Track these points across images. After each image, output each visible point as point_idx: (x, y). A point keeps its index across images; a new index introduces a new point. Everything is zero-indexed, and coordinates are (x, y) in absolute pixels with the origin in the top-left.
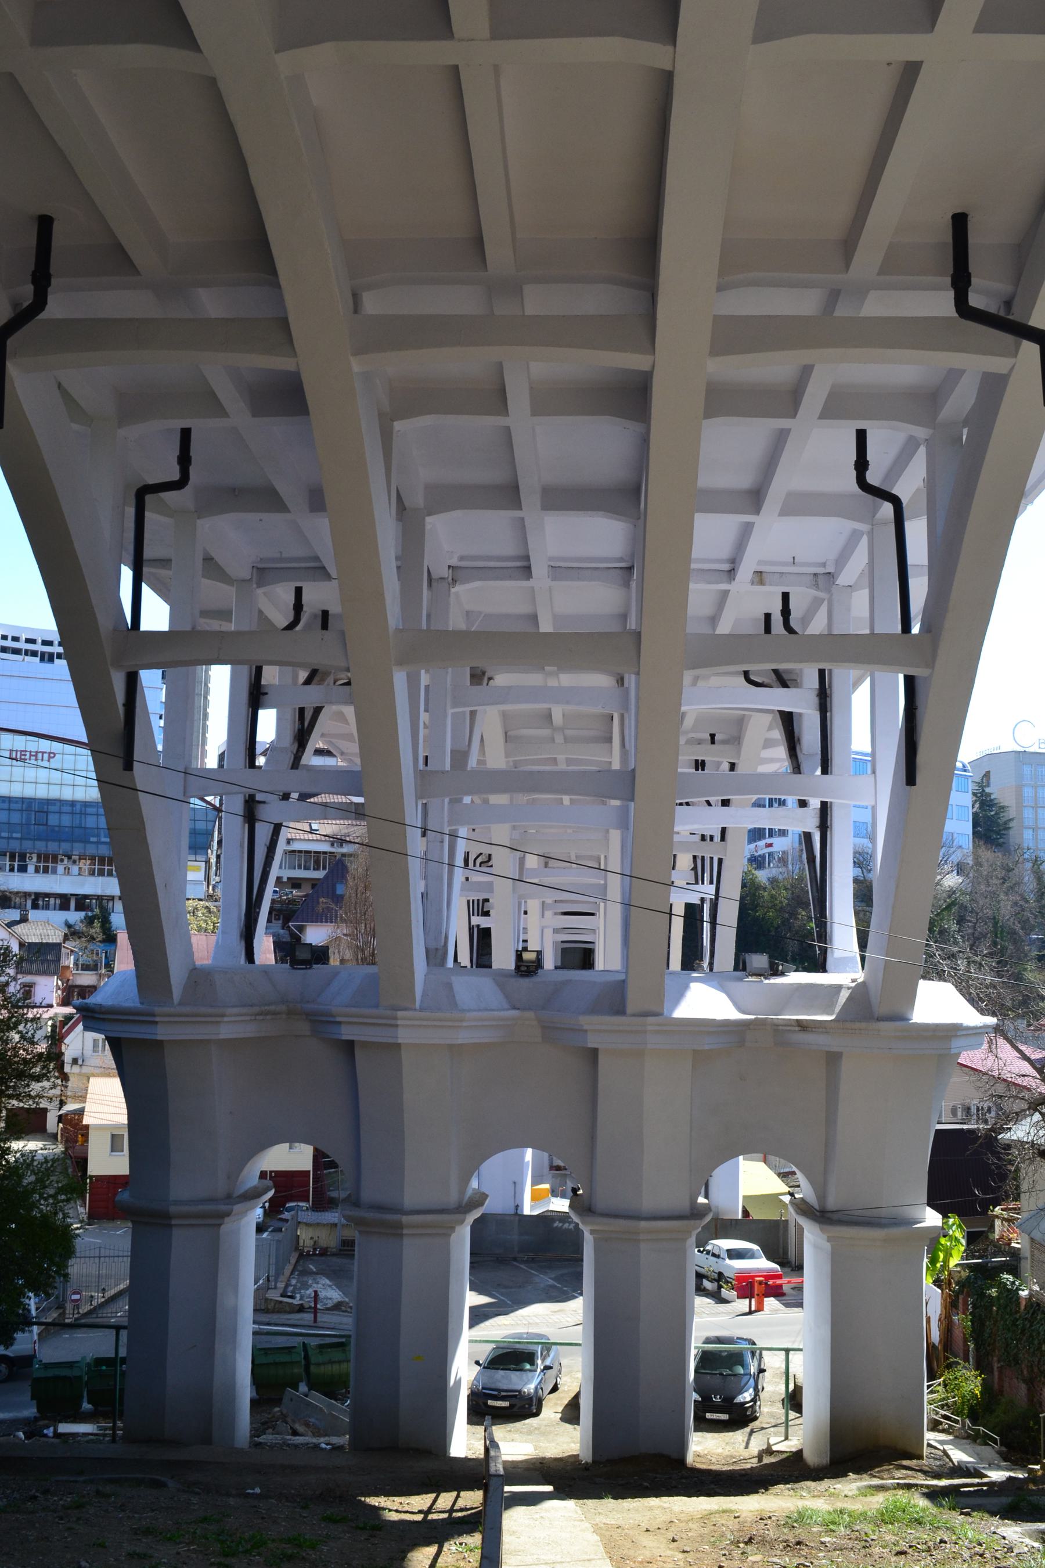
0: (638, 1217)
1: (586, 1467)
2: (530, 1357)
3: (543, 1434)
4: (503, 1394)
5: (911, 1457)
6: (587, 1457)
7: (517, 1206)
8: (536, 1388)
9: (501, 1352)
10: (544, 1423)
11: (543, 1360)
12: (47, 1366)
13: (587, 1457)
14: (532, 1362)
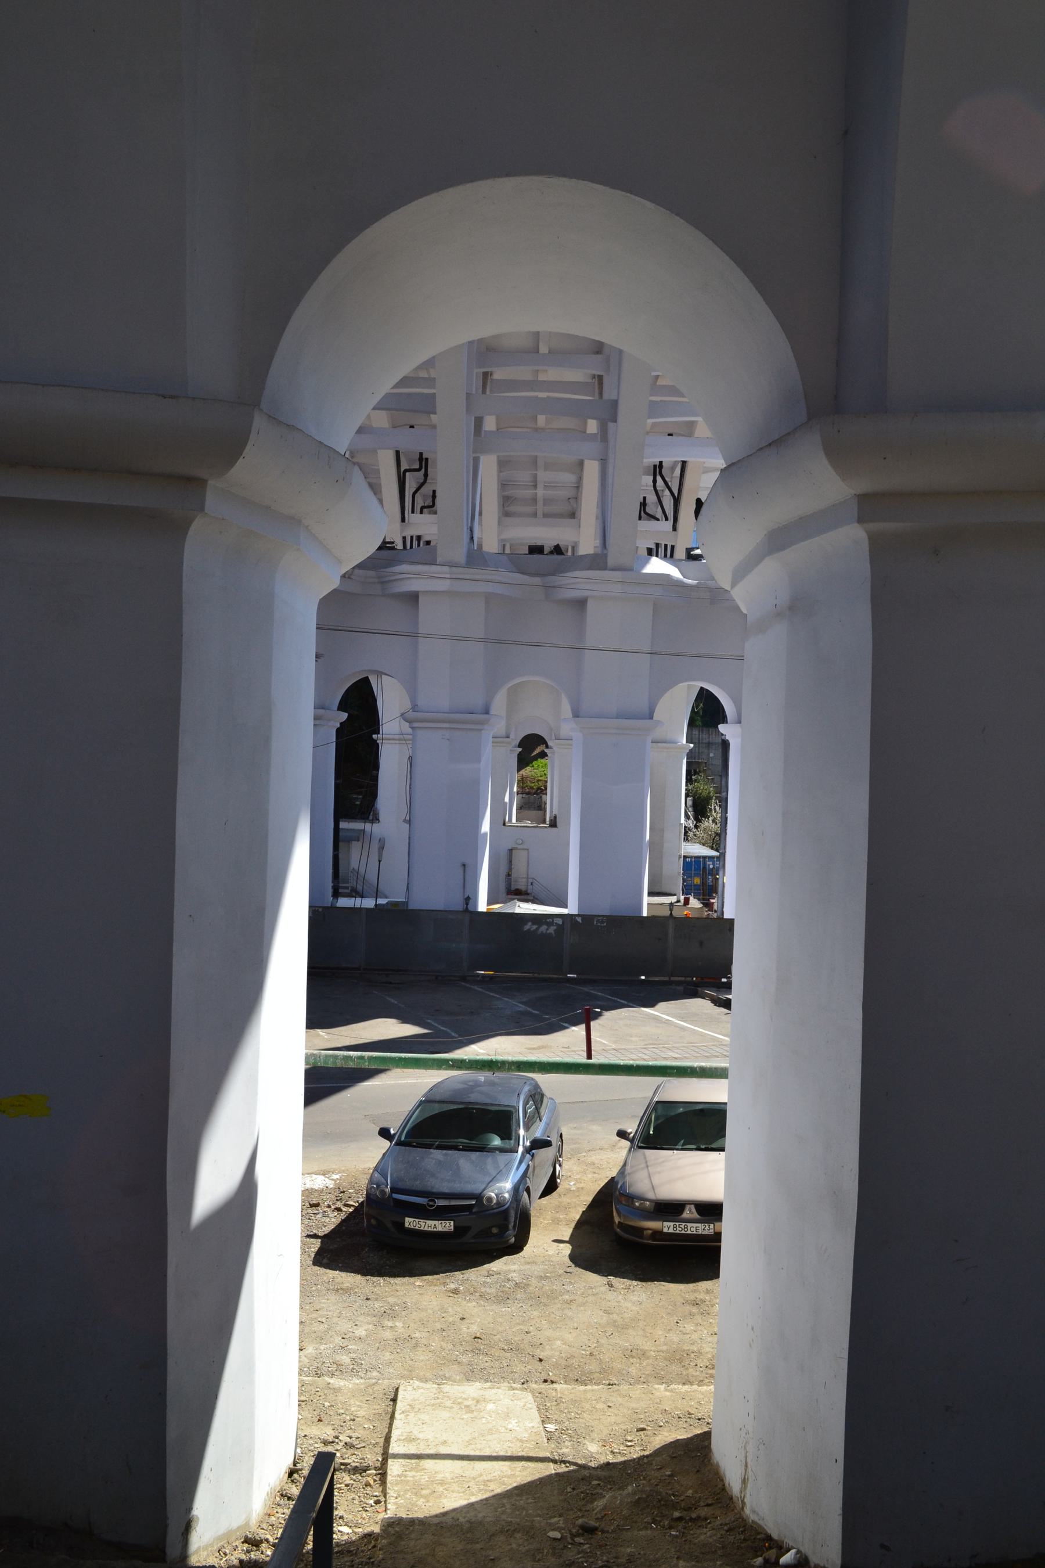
2: (501, 1122)
3: (537, 1300)
4: (441, 1203)
7: (467, 900)
8: (516, 1189)
9: (436, 1109)
10: (537, 1269)
11: (527, 1128)
14: (506, 1130)
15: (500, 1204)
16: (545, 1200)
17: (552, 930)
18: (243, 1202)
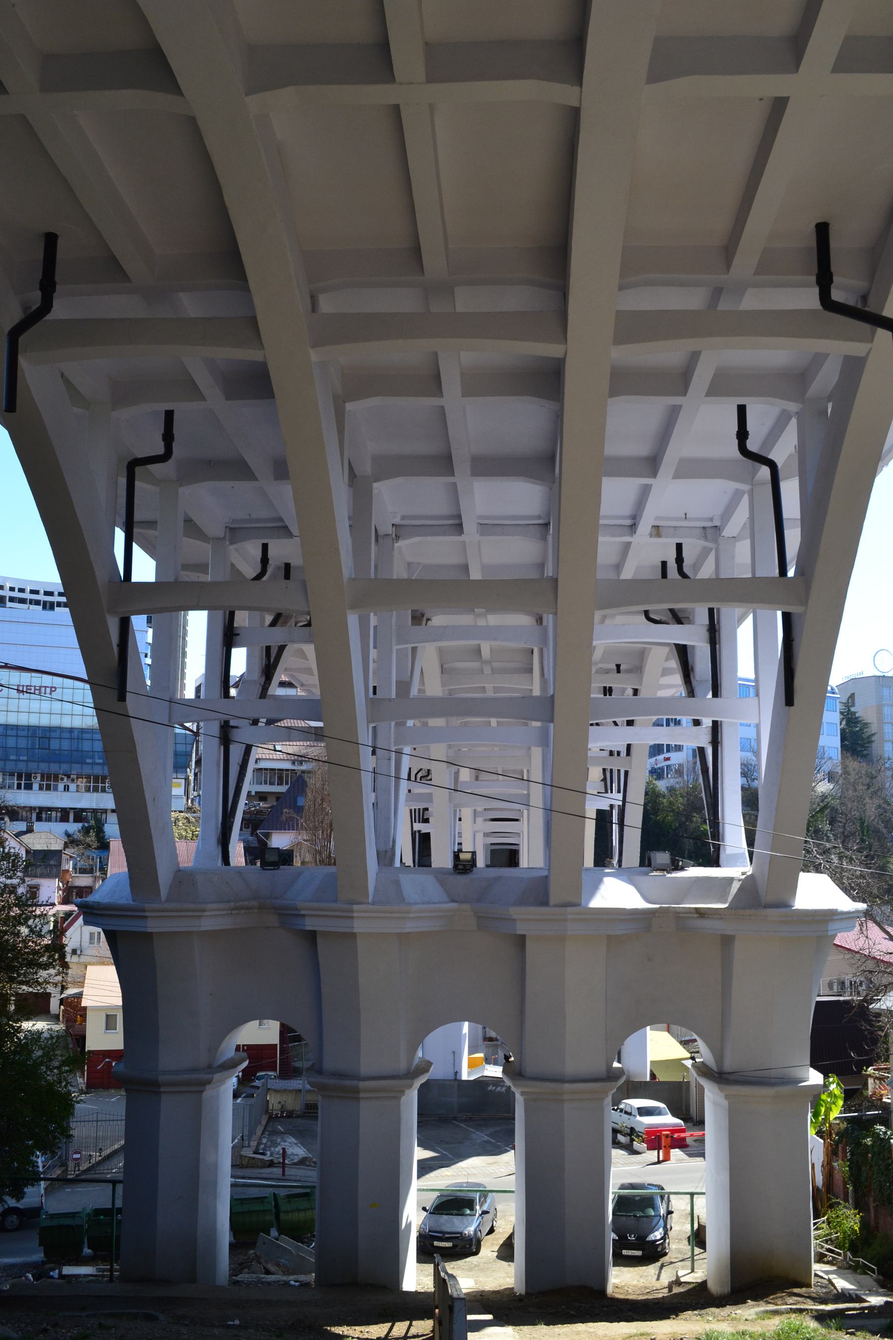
0: (561, 1080)
1: (520, 1298)
2: (469, 1204)
4: (447, 1236)
5: (801, 1286)
6: (521, 1289)
7: (456, 1073)
8: (475, 1230)
9: (444, 1199)
10: (483, 1260)
11: (481, 1206)
12: (52, 1216)
13: (521, 1289)
14: (472, 1208)
15: (469, 1236)
16: (489, 1236)
17: (504, 1089)
18: (409, 1226)
